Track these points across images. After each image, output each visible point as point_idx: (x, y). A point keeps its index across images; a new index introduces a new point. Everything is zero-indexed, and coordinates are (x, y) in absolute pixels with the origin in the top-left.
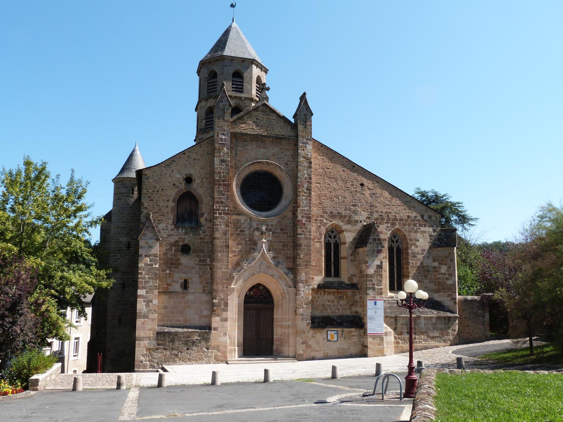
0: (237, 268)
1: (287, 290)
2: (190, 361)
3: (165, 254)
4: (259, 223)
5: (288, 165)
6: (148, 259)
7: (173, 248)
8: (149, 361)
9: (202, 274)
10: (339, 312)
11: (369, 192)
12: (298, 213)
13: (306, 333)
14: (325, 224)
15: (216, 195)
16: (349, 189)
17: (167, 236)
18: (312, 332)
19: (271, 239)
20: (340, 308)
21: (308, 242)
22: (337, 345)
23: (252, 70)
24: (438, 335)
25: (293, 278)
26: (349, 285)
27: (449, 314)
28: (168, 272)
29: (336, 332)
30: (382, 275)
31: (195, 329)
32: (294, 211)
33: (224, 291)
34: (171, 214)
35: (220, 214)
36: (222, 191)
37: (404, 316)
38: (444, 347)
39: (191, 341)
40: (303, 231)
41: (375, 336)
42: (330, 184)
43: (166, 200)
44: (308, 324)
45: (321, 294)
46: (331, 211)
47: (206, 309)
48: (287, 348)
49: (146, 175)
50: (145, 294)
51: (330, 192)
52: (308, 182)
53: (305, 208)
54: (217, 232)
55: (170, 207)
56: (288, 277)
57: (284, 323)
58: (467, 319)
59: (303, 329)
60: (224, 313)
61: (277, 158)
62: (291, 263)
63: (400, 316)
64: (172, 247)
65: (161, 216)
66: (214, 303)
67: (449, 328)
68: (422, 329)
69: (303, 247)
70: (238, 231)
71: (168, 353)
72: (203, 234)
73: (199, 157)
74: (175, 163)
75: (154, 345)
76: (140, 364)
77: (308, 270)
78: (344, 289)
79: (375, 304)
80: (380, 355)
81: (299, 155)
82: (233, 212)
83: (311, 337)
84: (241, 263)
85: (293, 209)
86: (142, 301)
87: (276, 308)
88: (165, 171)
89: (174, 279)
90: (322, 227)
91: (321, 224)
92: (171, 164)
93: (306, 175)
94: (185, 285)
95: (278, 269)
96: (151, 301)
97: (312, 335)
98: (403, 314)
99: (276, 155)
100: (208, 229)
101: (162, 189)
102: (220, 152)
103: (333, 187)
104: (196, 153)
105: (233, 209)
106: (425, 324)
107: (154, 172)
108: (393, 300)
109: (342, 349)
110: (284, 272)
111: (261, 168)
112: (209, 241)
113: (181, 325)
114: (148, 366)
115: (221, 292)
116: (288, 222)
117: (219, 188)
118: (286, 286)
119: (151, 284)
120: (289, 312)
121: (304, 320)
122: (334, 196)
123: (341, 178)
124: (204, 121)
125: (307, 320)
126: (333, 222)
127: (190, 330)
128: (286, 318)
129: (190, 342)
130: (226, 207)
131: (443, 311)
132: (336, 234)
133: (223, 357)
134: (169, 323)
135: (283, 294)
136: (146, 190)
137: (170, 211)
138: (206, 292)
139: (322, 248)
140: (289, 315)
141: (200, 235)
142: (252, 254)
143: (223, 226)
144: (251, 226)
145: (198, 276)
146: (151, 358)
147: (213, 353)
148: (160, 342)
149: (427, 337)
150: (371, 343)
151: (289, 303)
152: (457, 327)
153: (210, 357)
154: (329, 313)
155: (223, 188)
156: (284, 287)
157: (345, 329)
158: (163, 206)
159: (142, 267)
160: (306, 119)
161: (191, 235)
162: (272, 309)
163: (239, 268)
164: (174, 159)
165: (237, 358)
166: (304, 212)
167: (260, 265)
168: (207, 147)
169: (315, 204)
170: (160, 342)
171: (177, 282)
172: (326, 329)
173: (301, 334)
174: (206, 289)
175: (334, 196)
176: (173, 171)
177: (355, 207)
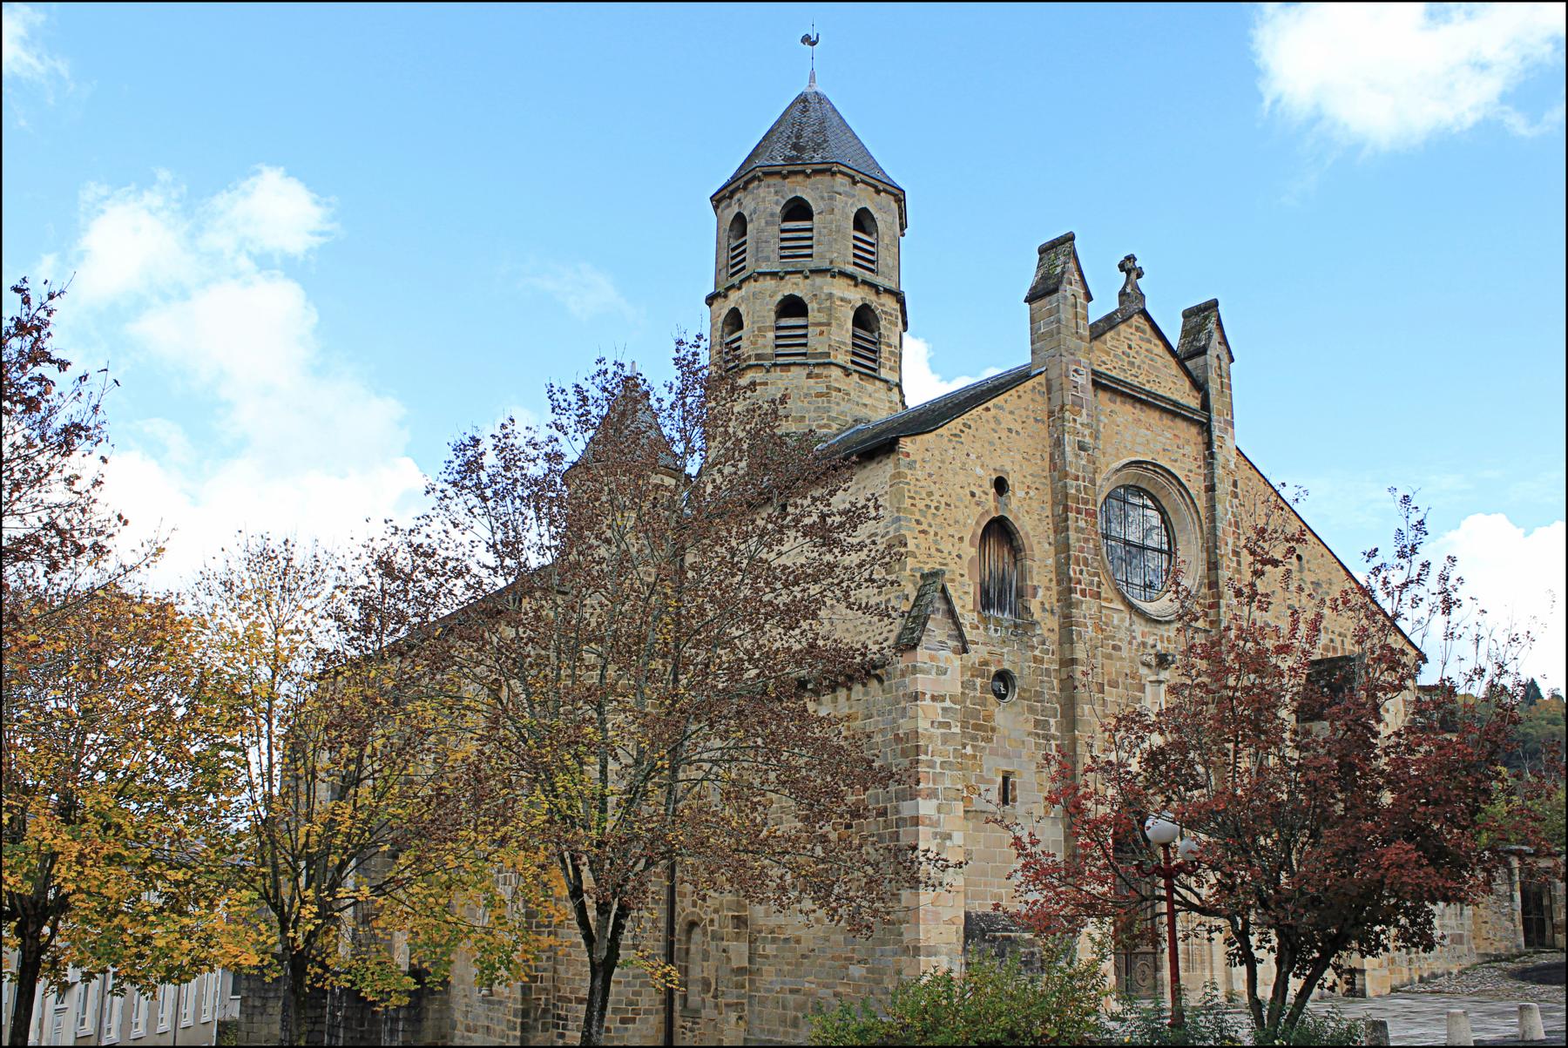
35: (1083, 593)
49: (908, 455)
55: (966, 558)
88: (951, 451)
96: (949, 837)
104: (1011, 413)
119: (948, 784)
124: (771, 335)
136: (911, 501)
155: (1086, 521)
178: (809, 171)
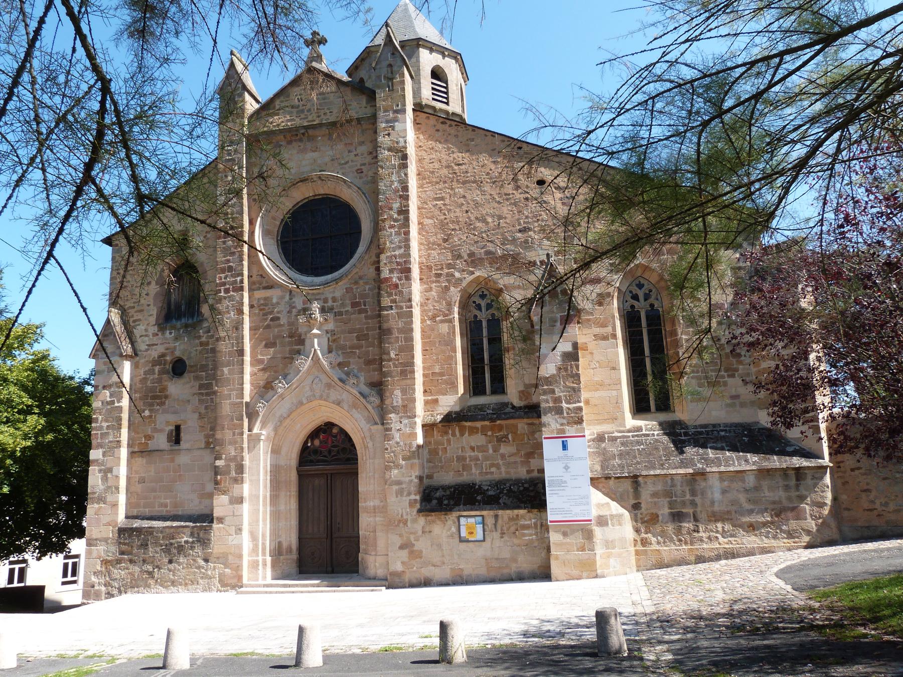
2: (174, 586)
3: (144, 381)
6: (107, 393)
8: (105, 585)
9: (203, 411)
10: (501, 473)
11: (558, 195)
13: (409, 524)
16: (511, 196)
18: (422, 520)
20: (501, 462)
22: (483, 551)
23: (418, 57)
24: (769, 519)
26: (520, 408)
27: (805, 463)
28: (147, 413)
29: (480, 519)
30: (578, 376)
35: (227, 291)
36: (230, 248)
37: (658, 472)
38: (789, 550)
39: (176, 545)
40: (394, 301)
41: (569, 528)
42: (466, 194)
44: (412, 504)
45: (454, 435)
46: (470, 250)
50: (101, 457)
52: (401, 197)
53: (397, 253)
56: (368, 402)
58: (860, 471)
59: (402, 516)
60: (235, 486)
61: (340, 164)
63: (644, 473)
67: (802, 498)
68: (716, 504)
69: (396, 334)
70: (266, 319)
71: (137, 569)
72: (205, 335)
75: (113, 554)
76: (90, 591)
78: (505, 419)
79: (565, 447)
80: (585, 574)
81: (380, 147)
83: (420, 532)
86: (97, 471)
89: (157, 426)
90: (452, 289)
91: (449, 281)
93: (396, 184)
94: (176, 436)
95: (347, 387)
97: (423, 527)
98: (654, 468)
105: (259, 278)
106: (724, 492)
108: (637, 436)
109: (497, 559)
110: (360, 393)
113: (168, 514)
114: (103, 595)
115: (230, 444)
116: (367, 287)
117: (224, 243)
118: (368, 423)
121: (402, 496)
123: (491, 178)
125: (409, 494)
126: (477, 274)
127: (175, 524)
129: (175, 547)
131: (783, 453)
132: (492, 301)
134: (147, 510)
137: (152, 302)
139: (454, 333)
141: (200, 337)
145: (196, 416)
146: (108, 579)
147: (215, 570)
148: (124, 547)
149: (733, 526)
150: (560, 545)
152: (829, 496)
154: (474, 475)
157: (500, 512)
159: (98, 408)
160: (392, 73)
162: (355, 474)
163: (271, 393)
165: (269, 581)
166: (394, 260)
170: (124, 547)
172: (455, 514)
173: (398, 525)
174: (211, 440)
175: (477, 218)
177: (526, 235)
178: (447, 53)
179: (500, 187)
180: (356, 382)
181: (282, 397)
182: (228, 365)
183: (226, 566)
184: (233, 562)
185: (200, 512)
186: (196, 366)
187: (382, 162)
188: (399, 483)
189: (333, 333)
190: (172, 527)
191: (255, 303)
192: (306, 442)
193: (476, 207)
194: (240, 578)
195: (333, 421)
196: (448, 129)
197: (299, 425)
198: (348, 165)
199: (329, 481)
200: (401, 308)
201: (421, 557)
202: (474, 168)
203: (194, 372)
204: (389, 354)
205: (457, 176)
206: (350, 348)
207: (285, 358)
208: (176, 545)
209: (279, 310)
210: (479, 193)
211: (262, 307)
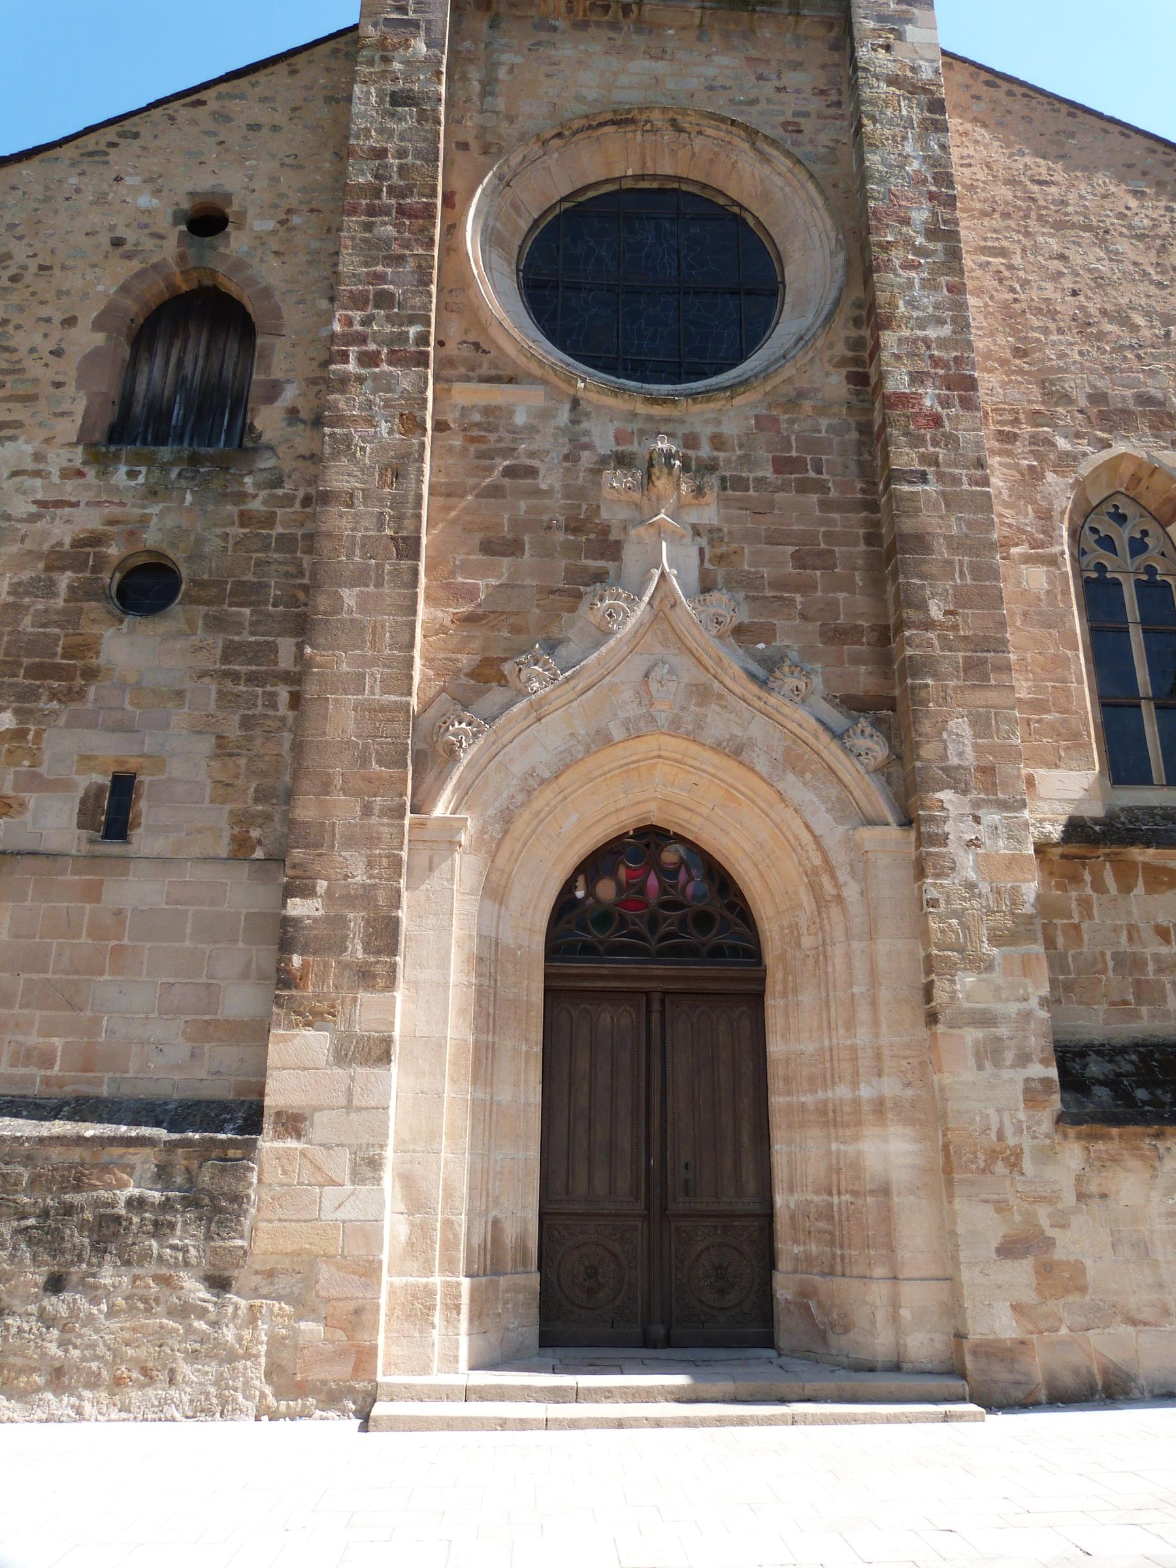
0: (480, 694)
1: (850, 844)
4: (629, 427)
5: (800, 131)
7: (64, 580)
9: (233, 731)
12: (885, 356)
13: (1027, 1164)
14: (1066, 462)
15: (350, 263)
17: (33, 509)
19: (715, 522)
21: (969, 524)
25: (888, 762)
31: (128, 1124)
32: (857, 361)
33: (372, 840)
34: (79, 387)
36: (387, 242)
39: (88, 1215)
42: (1067, 253)
43: (58, 317)
44: (1033, 1095)
45: (1099, 886)
47: (245, 975)
48: (878, 1292)
51: (1075, 293)
52: (932, 197)
53: (931, 333)
54: (345, 461)
56: (848, 751)
57: (842, 1092)
59: (1001, 1137)
60: (362, 995)
62: (863, 668)
64: (55, 575)
65: (11, 405)
66: (295, 922)
69: (942, 551)
72: (263, 494)
73: (280, 118)
74: (136, 143)
77: (993, 697)
81: (866, 70)
82: (463, 370)
83: (1070, 1198)
84: (507, 668)
85: (850, 354)
87: (779, 987)
88: (73, 180)
89: (43, 770)
90: (1050, 477)
92: (112, 150)
93: (916, 165)
95: (772, 700)
97: (1079, 1179)
99: (723, 87)
100: (300, 463)
101: (41, 268)
102: (386, 60)
103: (1090, 270)
104: (264, 100)
105: (467, 352)
107: (13, 188)
110: (818, 720)
111: (644, 164)
112: (299, 533)
113: (55, 1091)
115: (351, 841)
116: (824, 423)
117: (368, 227)
118: (839, 820)
120: (874, 1004)
121: (997, 1064)
122: (1104, 312)
125: (1023, 1059)
126: (1120, 448)
127: (90, 1130)
128: (853, 1049)
129: (82, 1226)
130: (412, 320)
132: (1145, 533)
133: (341, 1354)
135: (825, 880)
138: (259, 854)
139: (1066, 593)
140: (876, 1023)
141: (242, 497)
142: (583, 607)
143: (384, 426)
144: (577, 445)
145: (206, 745)
151: (871, 936)
153: (232, 1357)
156: (823, 821)
158: (32, 350)
161: (189, 497)
162: (755, 999)
163: (496, 696)
164: (136, 125)
167: (647, 676)
168: (328, 70)
169: (988, 355)
171: (60, 785)
176: (118, 179)
179: (1158, 252)
180: (802, 686)
181: (538, 712)
182: (359, 578)
183: (303, 1306)
184: (334, 1293)
185: (189, 1095)
186: (221, 584)
187: (874, 104)
188: (984, 1019)
189: (714, 535)
190: (80, 1141)
191: (451, 418)
192: (569, 886)
193: (1099, 286)
194: (365, 1358)
195: (657, 818)
196: (1006, 100)
197: (574, 818)
198: (758, 107)
199: (656, 1017)
200: (956, 481)
201: (1082, 1289)
202: (1081, 197)
203: (208, 603)
204: (923, 607)
205: (1039, 208)
206: (772, 585)
207: (552, 592)
208: (88, 1215)
209: (534, 447)
210: (1102, 255)
211: (475, 433)
